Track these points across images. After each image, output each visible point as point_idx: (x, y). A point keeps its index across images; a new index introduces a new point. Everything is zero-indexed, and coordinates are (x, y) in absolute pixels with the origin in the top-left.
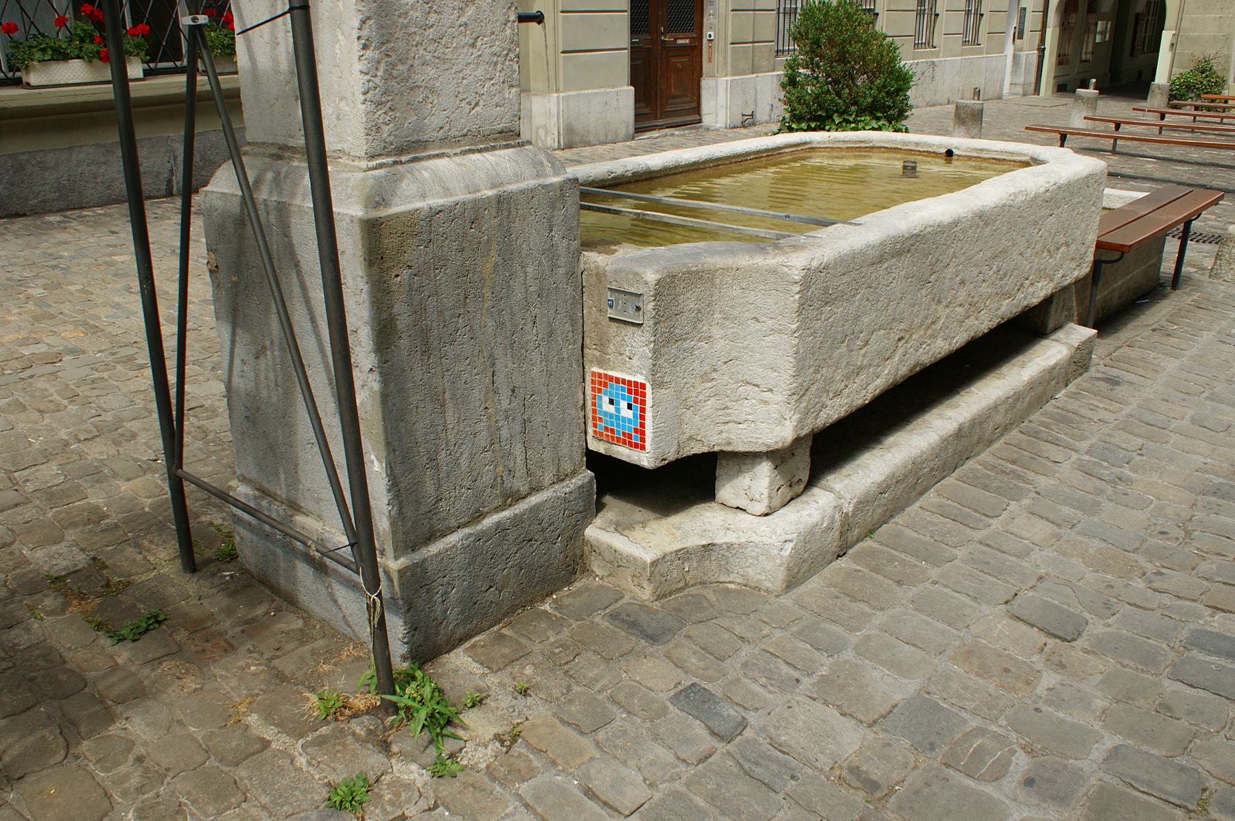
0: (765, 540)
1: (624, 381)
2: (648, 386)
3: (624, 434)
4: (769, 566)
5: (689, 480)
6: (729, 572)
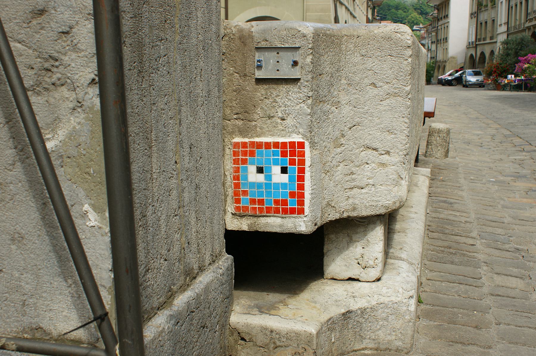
0: (393, 299)
1: (276, 145)
2: (307, 144)
3: (276, 202)
4: (398, 324)
6: (362, 338)
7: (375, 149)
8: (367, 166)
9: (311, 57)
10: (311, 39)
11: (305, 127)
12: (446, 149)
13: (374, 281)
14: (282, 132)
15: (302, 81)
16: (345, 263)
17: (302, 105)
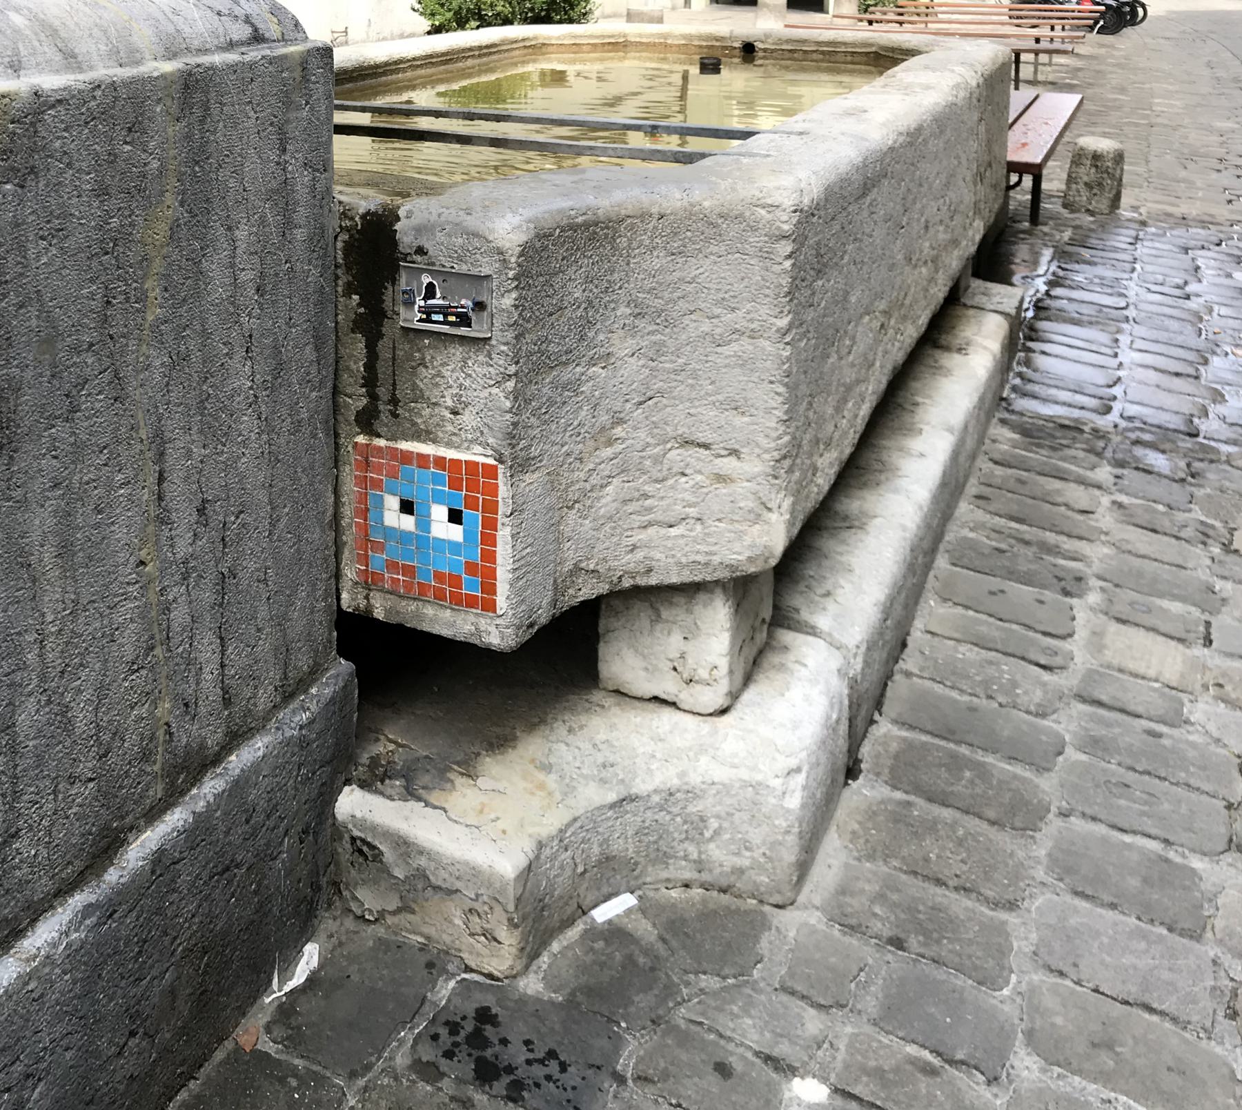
3: (439, 576)
5: (564, 656)
7: (706, 446)
8: (684, 479)
9: (514, 295)
10: (513, 260)
11: (500, 436)
12: (1114, 192)
13: (711, 715)
14: (454, 438)
15: (493, 342)
16: (644, 664)
17: (495, 390)
